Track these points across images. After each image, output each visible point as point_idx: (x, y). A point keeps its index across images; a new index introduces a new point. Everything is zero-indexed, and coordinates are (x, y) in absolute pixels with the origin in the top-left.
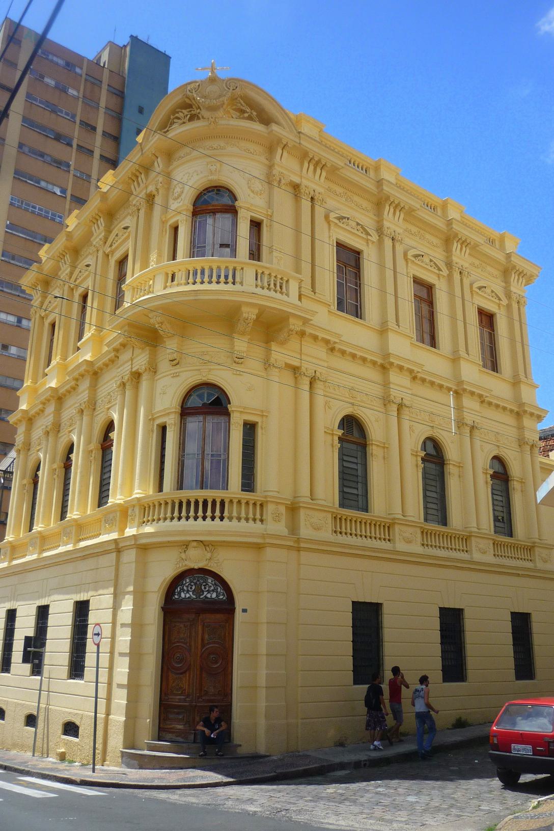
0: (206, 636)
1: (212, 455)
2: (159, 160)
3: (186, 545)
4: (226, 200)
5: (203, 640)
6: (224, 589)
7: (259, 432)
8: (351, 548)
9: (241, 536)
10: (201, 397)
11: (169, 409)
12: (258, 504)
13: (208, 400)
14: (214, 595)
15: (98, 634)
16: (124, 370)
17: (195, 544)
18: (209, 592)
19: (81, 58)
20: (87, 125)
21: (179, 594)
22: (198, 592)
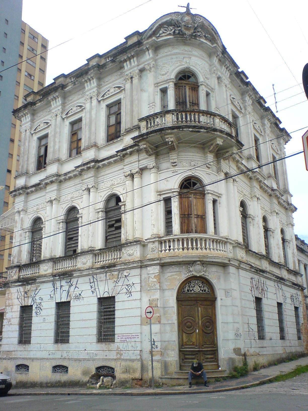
3: (192, 263)
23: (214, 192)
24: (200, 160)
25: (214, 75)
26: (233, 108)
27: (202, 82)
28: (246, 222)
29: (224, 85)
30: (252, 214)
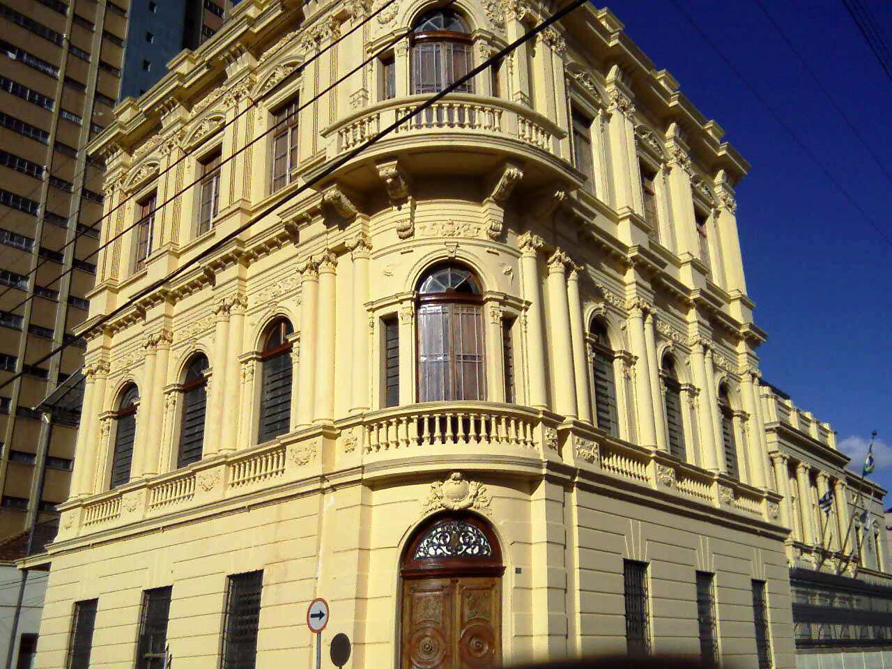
0: (467, 611)
1: (465, 357)
5: (462, 615)
9: (517, 463)
10: (443, 280)
15: (321, 615)
18: (469, 545)
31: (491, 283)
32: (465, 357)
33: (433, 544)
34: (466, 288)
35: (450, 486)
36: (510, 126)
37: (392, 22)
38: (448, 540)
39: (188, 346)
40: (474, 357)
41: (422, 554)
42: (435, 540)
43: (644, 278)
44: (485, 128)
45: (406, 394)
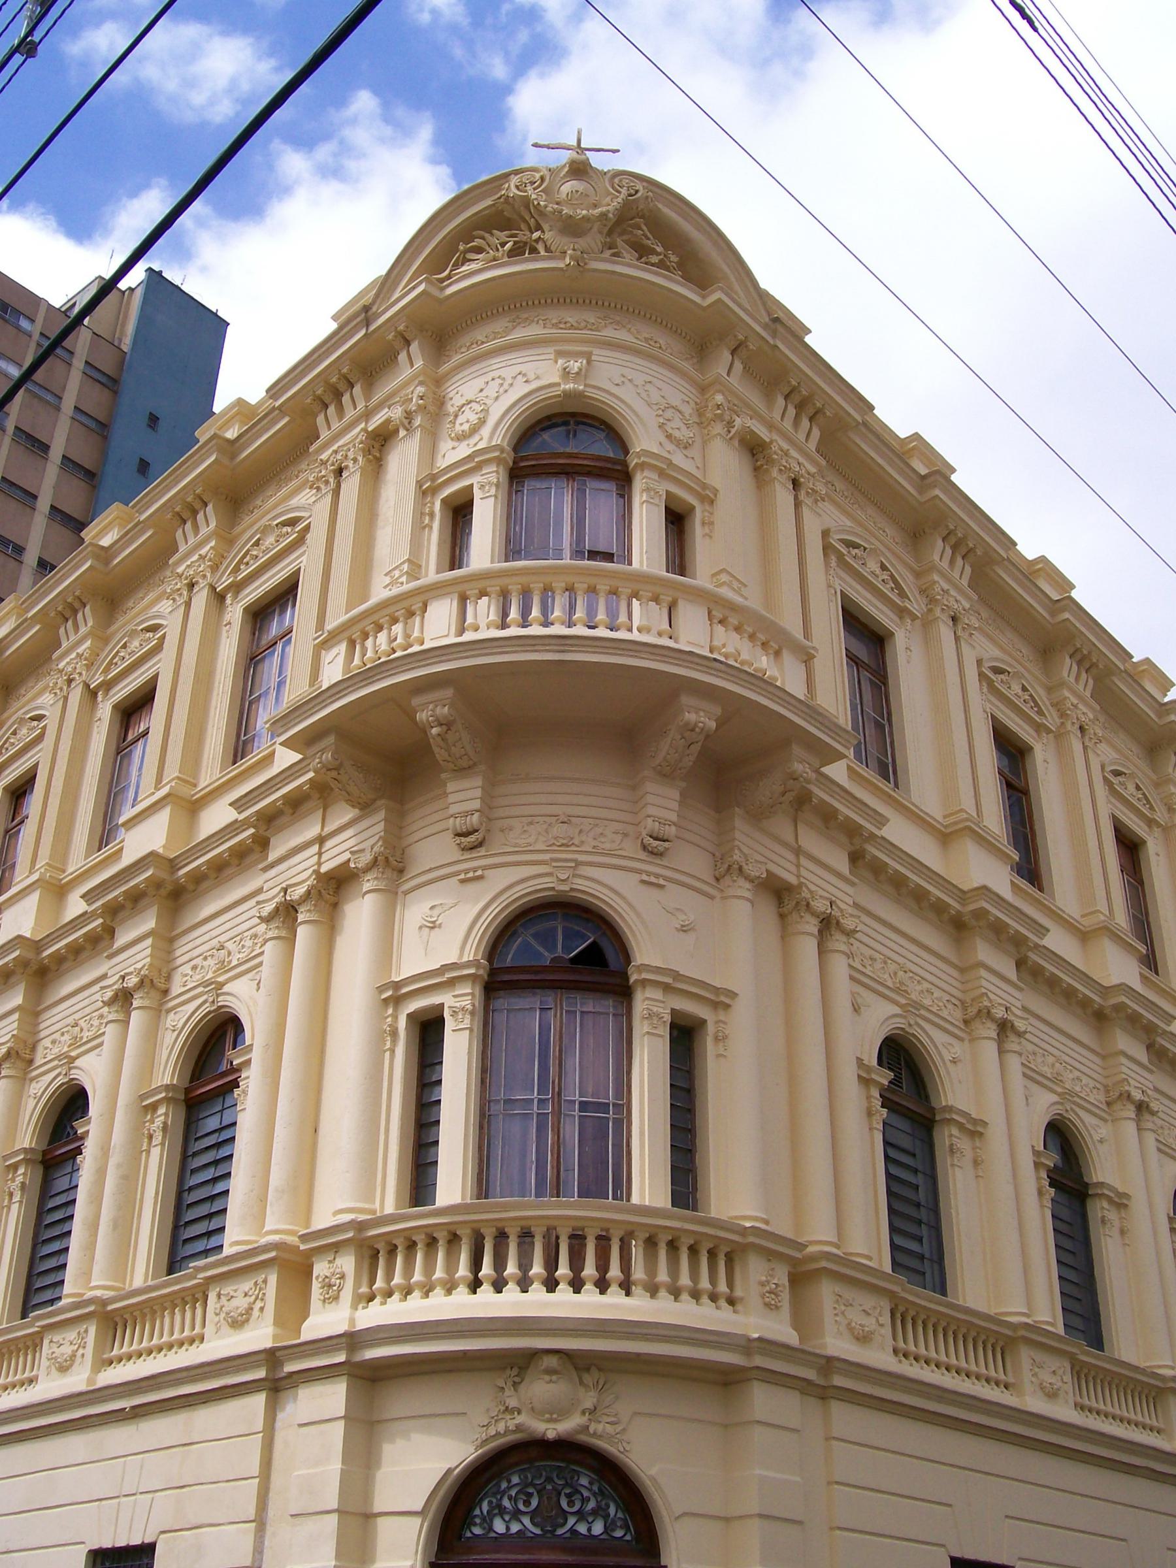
2: (210, 508)
3: (517, 1365)
4: (602, 448)
6: (627, 1509)
7: (710, 1048)
8: (940, 1399)
11: (453, 966)
12: (723, 1250)
13: (567, 949)
14: (598, 1528)
16: (294, 867)
17: (552, 1361)
18: (581, 1515)
19: (35, 300)
20: (29, 437)
21: (487, 1522)
22: (549, 1516)
23: (677, 976)
24: (604, 813)
25: (718, 428)
26: (1118, 814)
27: (646, 453)
28: (1084, 1216)
29: (945, 617)
30: (1109, 1180)
31: (650, 949)
32: (584, 1106)
33: (502, 1511)
34: (593, 957)
35: (542, 1387)
36: (694, 632)
37: (476, 438)
38: (534, 1502)
39: (56, 1072)
40: (604, 1107)
41: (477, 1531)
42: (506, 1503)
43: (773, 623)
44: (639, 630)
45: (452, 1184)
